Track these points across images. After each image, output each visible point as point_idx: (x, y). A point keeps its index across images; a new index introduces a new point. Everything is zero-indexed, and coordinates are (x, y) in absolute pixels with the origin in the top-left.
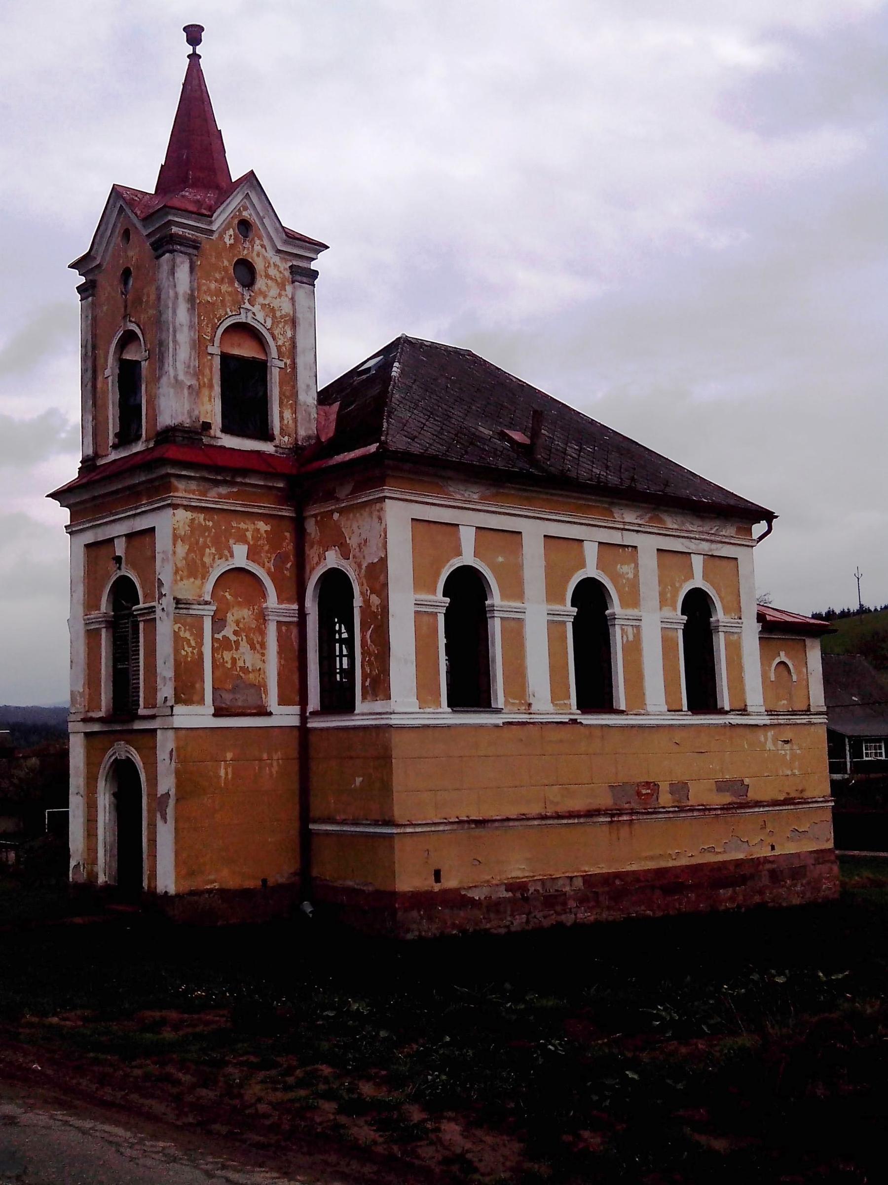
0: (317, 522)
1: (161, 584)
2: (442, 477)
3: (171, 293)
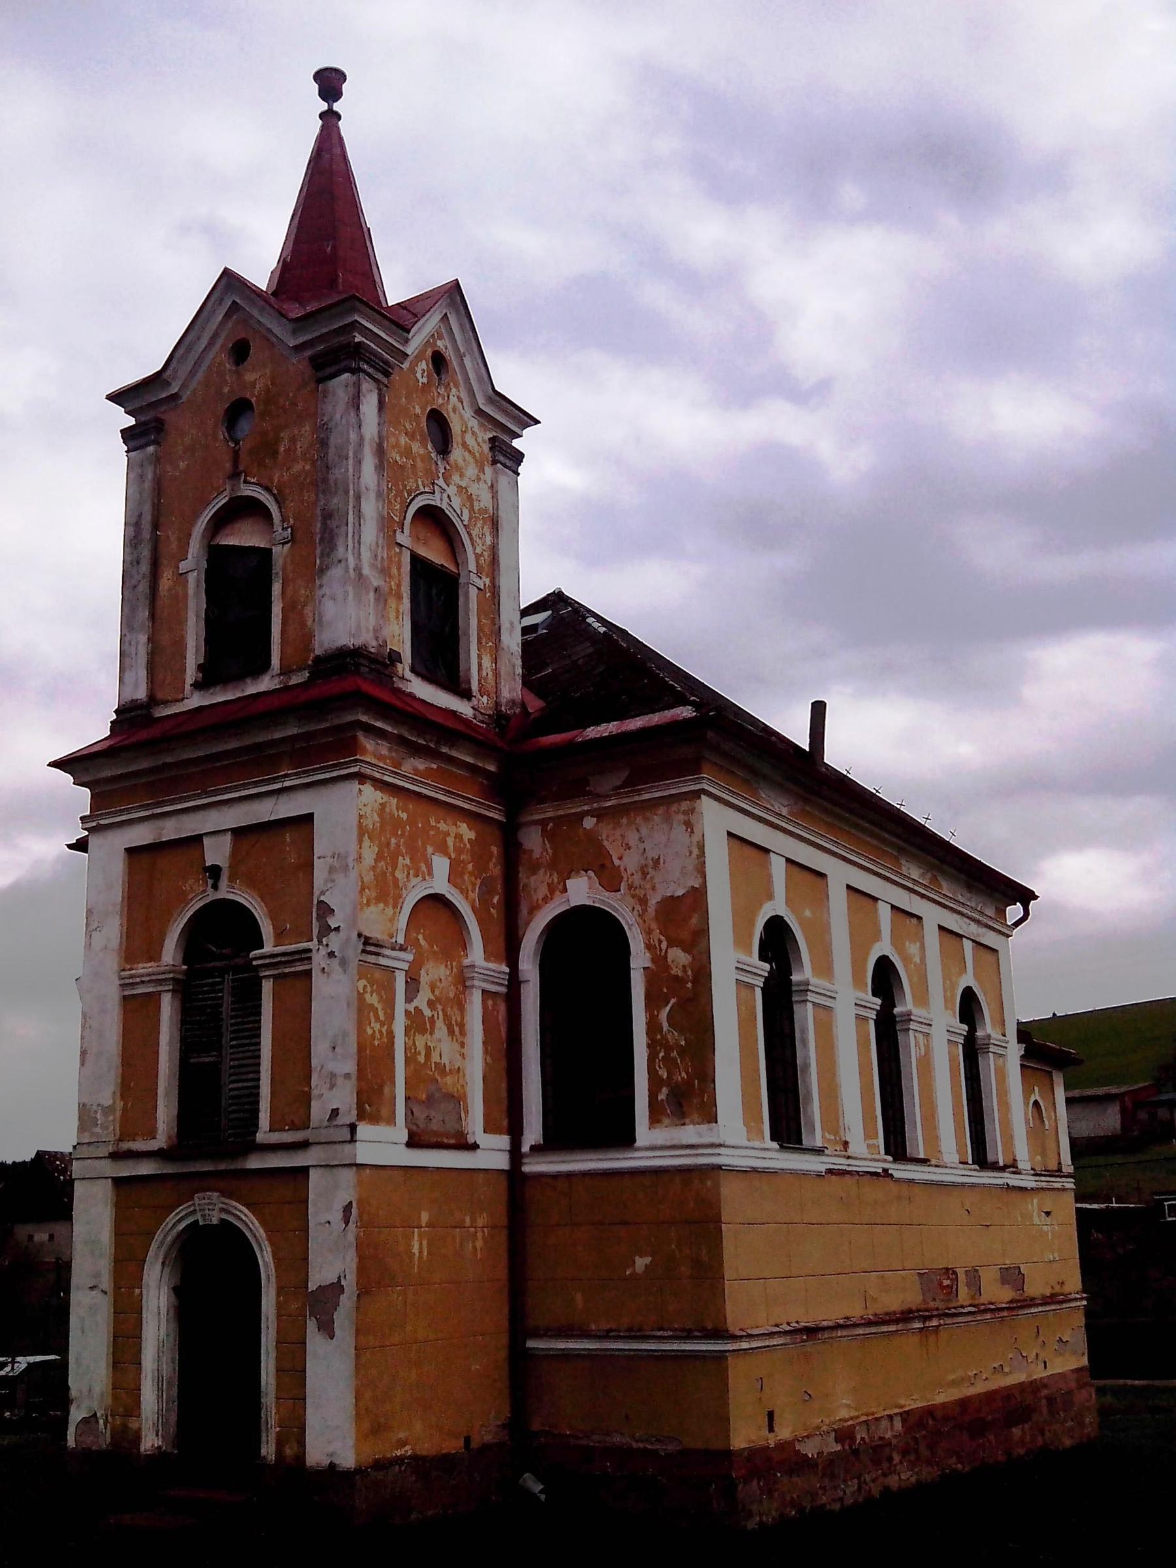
0: (544, 831)
1: (326, 910)
2: (755, 773)
3: (353, 436)
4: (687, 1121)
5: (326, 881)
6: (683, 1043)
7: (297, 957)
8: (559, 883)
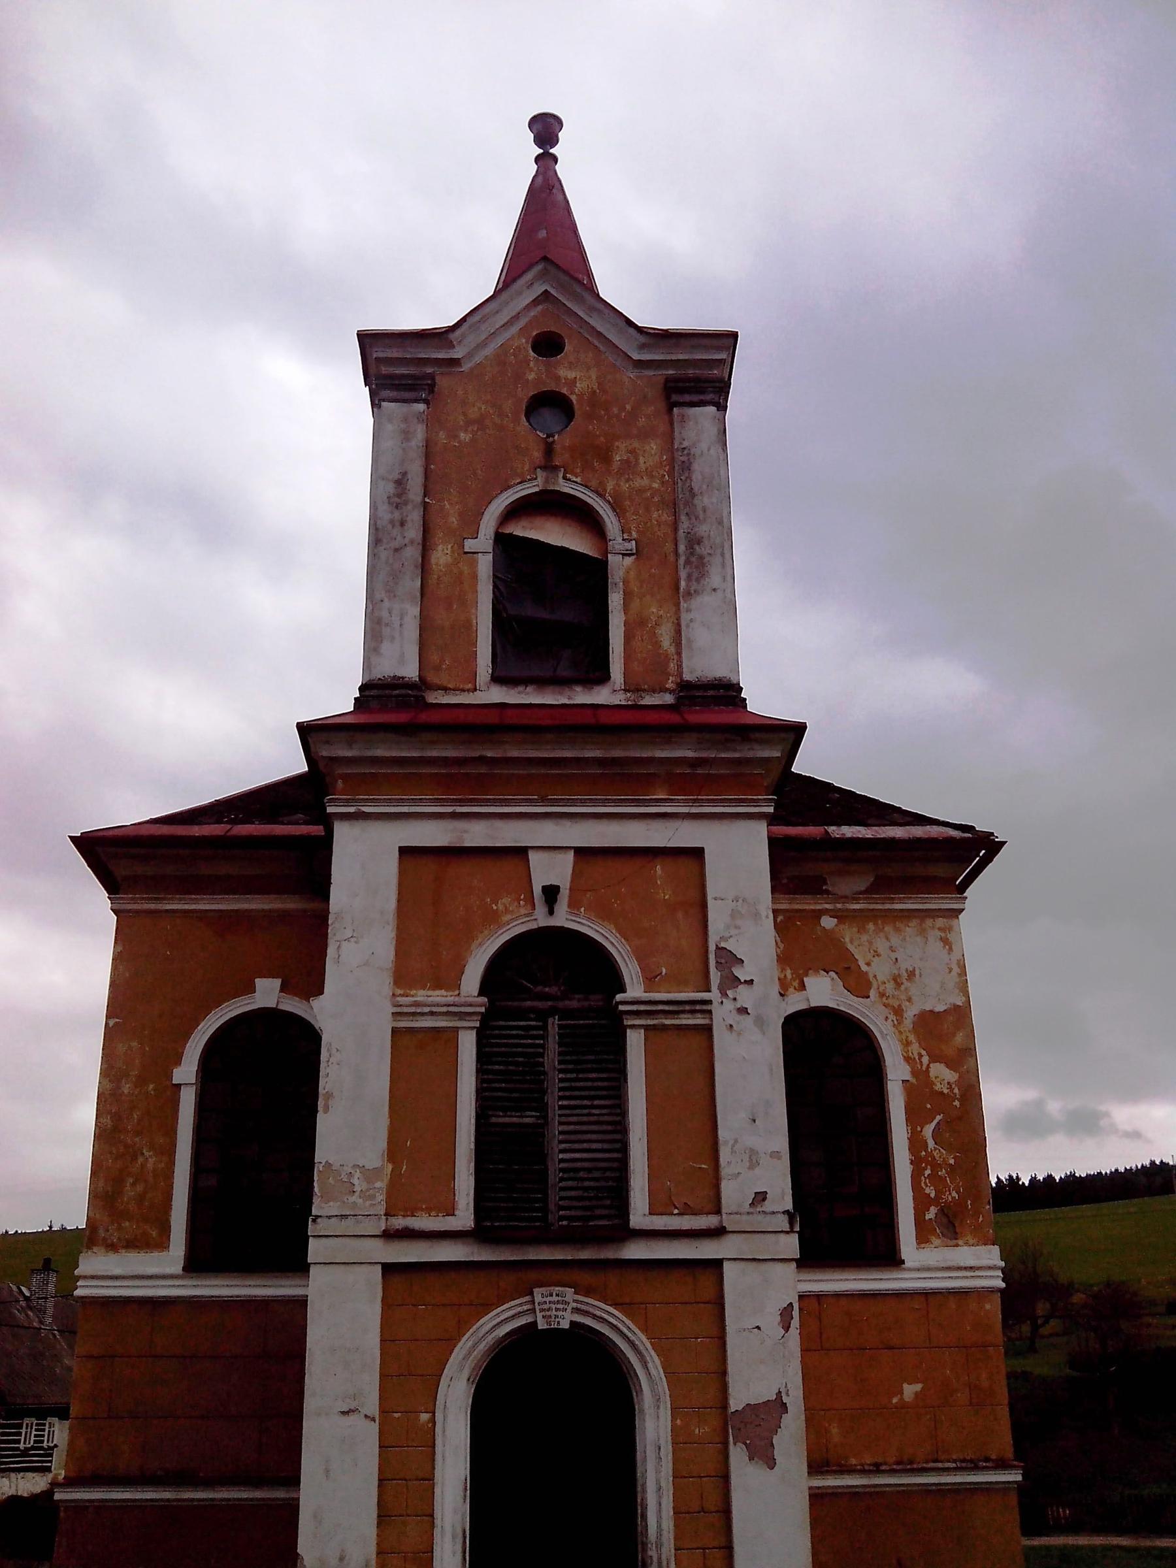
1: (728, 959)
4: (960, 1242)
5: (728, 927)
6: (952, 1161)
7: (687, 1008)
8: (793, 979)
